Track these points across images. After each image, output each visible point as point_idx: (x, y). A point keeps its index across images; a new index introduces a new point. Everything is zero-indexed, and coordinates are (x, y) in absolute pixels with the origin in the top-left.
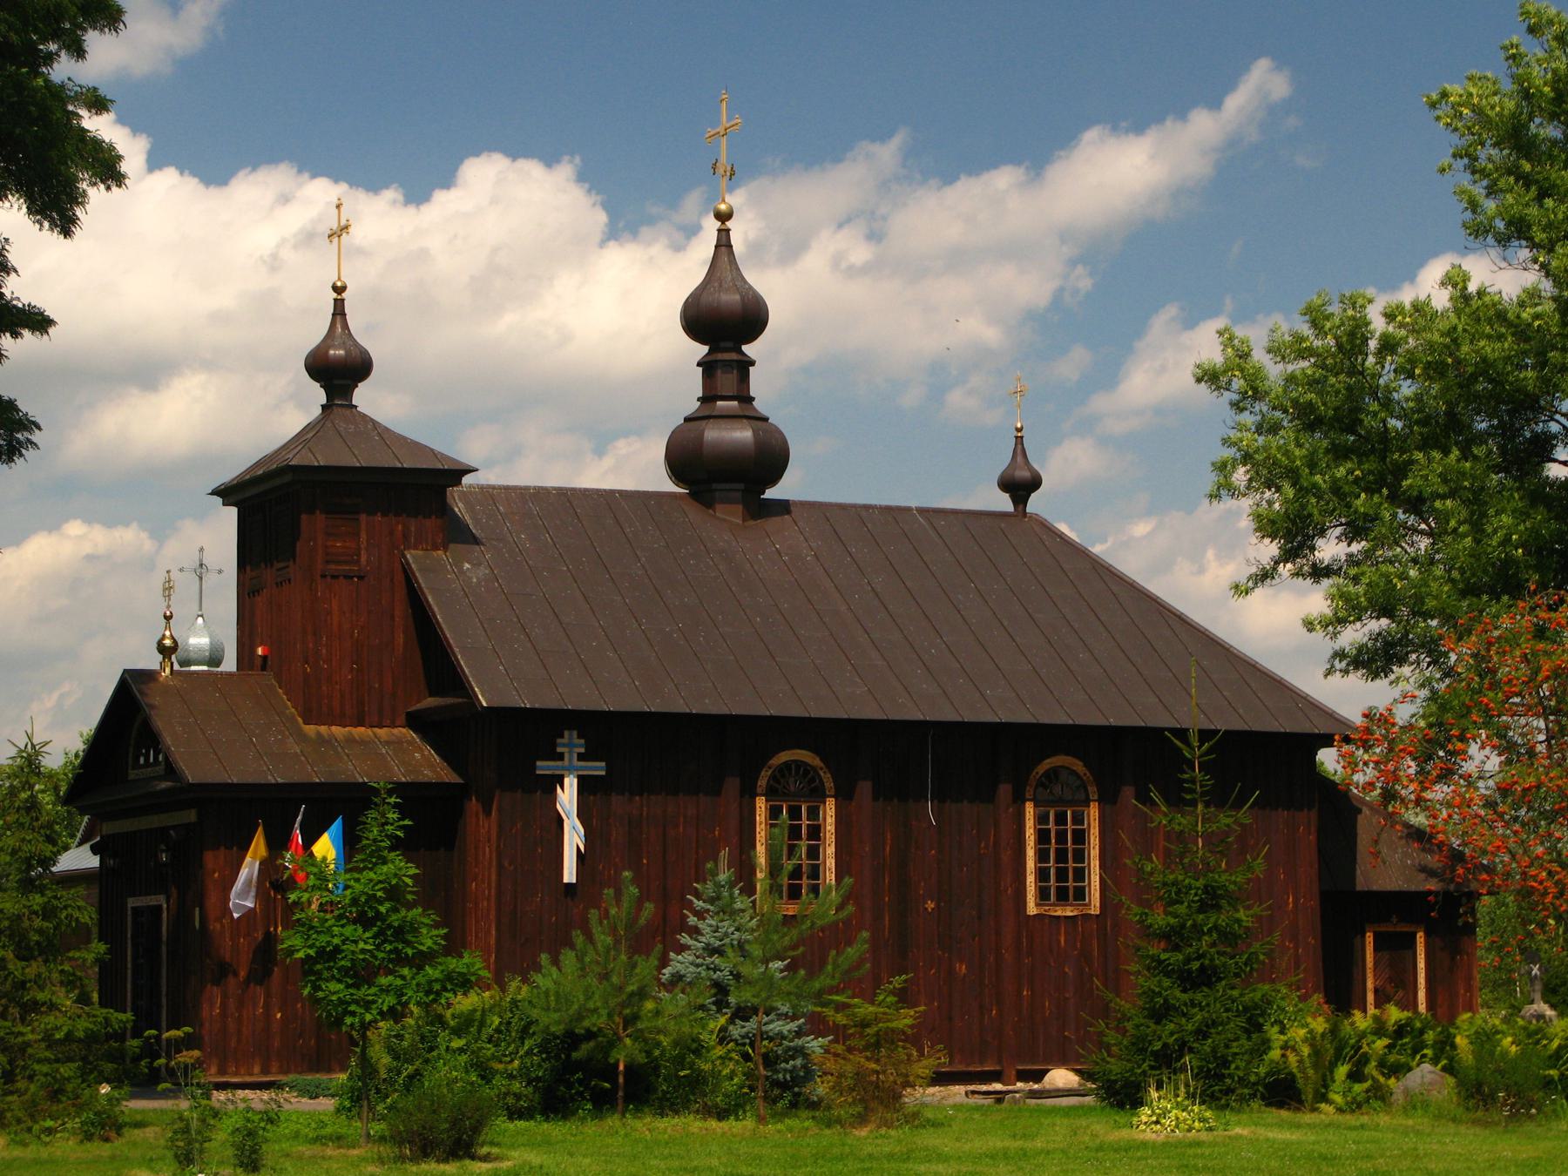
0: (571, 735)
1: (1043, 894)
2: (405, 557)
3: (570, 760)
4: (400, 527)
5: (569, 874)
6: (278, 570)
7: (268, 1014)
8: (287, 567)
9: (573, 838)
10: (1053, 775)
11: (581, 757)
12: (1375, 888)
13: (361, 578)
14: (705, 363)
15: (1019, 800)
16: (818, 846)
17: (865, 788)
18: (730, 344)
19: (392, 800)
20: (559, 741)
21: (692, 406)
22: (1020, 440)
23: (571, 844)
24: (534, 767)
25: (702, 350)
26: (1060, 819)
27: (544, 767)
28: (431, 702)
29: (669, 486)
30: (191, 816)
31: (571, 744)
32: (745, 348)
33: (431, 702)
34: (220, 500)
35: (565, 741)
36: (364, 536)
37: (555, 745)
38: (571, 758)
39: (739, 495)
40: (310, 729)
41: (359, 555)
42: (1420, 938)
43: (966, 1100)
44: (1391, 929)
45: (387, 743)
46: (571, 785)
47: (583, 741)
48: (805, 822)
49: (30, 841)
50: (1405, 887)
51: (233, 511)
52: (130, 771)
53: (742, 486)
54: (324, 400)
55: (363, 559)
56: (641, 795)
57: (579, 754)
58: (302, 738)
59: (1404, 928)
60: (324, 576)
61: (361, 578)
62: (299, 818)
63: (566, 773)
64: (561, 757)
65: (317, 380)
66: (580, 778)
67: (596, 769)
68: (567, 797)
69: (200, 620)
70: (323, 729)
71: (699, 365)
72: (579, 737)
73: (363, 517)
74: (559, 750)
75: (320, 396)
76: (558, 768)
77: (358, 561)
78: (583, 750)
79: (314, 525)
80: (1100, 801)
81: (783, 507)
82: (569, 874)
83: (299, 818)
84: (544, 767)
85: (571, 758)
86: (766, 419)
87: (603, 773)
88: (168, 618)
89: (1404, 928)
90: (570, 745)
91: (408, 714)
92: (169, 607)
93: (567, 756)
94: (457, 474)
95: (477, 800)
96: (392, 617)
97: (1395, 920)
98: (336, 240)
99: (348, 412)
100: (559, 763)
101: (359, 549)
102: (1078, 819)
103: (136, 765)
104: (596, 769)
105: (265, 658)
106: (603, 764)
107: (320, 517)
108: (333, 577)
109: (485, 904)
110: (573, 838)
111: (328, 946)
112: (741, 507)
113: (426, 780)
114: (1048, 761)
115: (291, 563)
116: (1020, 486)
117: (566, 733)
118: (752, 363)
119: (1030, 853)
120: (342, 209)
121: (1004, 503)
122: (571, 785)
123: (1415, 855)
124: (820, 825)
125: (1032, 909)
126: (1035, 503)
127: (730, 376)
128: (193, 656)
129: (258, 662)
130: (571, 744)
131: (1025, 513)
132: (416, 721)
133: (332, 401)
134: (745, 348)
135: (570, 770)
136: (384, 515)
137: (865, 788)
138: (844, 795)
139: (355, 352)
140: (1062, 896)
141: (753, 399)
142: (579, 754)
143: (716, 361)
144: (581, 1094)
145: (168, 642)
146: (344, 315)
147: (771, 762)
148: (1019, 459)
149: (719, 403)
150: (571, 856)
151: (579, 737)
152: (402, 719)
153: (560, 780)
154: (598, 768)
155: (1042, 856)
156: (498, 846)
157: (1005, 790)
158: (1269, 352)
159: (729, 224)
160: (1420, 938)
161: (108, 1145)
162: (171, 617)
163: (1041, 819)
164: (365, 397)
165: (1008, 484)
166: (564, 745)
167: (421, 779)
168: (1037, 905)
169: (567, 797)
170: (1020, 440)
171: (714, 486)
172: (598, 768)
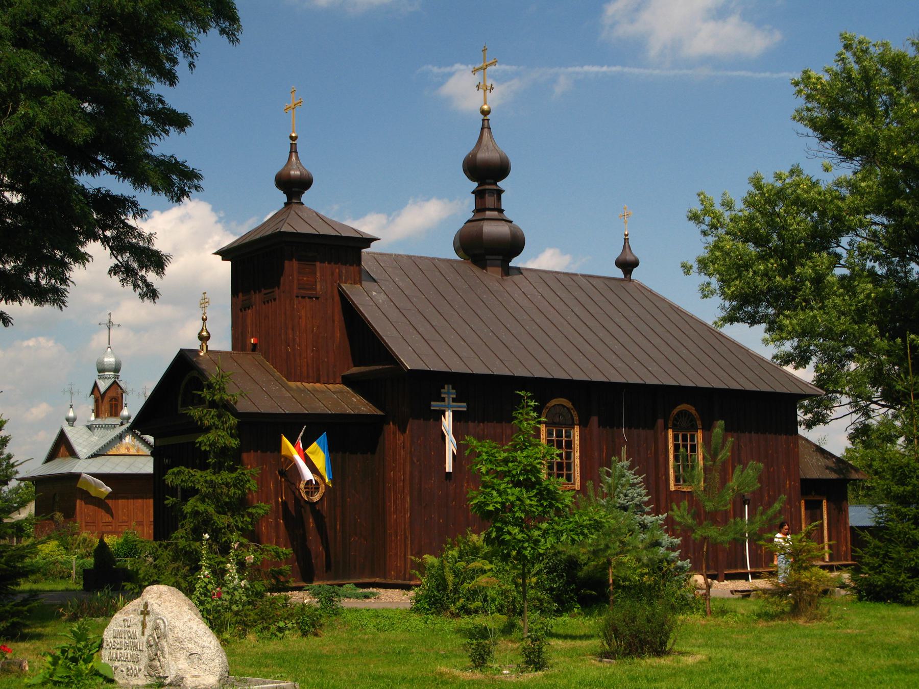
0: (448, 388)
1: (677, 480)
2: (341, 287)
3: (449, 403)
4: (337, 270)
5: (449, 467)
6: (265, 294)
8: (273, 292)
9: (451, 446)
10: (682, 413)
11: (454, 400)
12: (808, 477)
13: (317, 298)
14: (478, 191)
15: (666, 428)
16: (182, 489)
17: (594, 420)
18: (492, 181)
19: (533, 404)
20: (442, 390)
21: (470, 215)
22: (626, 240)
23: (449, 450)
24: (430, 405)
25: (475, 185)
26: (685, 439)
27: (435, 405)
28: (355, 370)
31: (448, 393)
33: (355, 370)
34: (220, 257)
35: (445, 390)
36: (318, 275)
37: (440, 393)
38: (449, 400)
39: (499, 262)
40: (292, 384)
41: (316, 286)
42: (824, 503)
43: (731, 596)
44: (812, 498)
45: (334, 393)
46: (449, 415)
47: (454, 391)
48: (564, 439)
49: (223, 437)
50: (821, 477)
53: (501, 257)
55: (318, 287)
56: (483, 423)
57: (453, 398)
58: (289, 389)
59: (818, 498)
60: (297, 297)
61: (317, 298)
62: (302, 433)
63: (446, 409)
64: (443, 400)
66: (454, 412)
67: (462, 407)
68: (447, 422)
69: (109, 349)
70: (299, 384)
71: (473, 193)
72: (453, 389)
73: (318, 264)
74: (443, 396)
75: (284, 198)
76: (442, 406)
77: (315, 289)
78: (454, 396)
79: (292, 267)
80: (702, 429)
81: (519, 270)
82: (449, 467)
83: (302, 433)
84: (435, 405)
85: (449, 400)
86: (511, 222)
87: (465, 409)
89: (818, 498)
90: (448, 393)
92: (204, 314)
93: (446, 399)
94: (367, 241)
95: (393, 424)
96: (333, 321)
97: (813, 494)
99: (301, 206)
100: (443, 403)
101: (316, 282)
102: (692, 439)
104: (462, 407)
105: (255, 345)
106: (465, 404)
107: (295, 264)
108: (303, 297)
109: (401, 484)
110: (451, 446)
111: (507, 502)
112: (500, 269)
113: (364, 413)
114: (685, 405)
115: (277, 288)
116: (627, 265)
117: (446, 386)
119: (671, 457)
121: (619, 273)
122: (449, 416)
123: (823, 462)
124: (571, 441)
126: (636, 274)
127: (492, 198)
128: (107, 367)
129: (249, 347)
130: (448, 393)
131: (630, 280)
132: (348, 381)
133: (292, 199)
135: (449, 407)
136: (329, 263)
137: (594, 420)
138: (584, 424)
139: (305, 173)
141: (503, 210)
142: (453, 398)
143: (485, 190)
144: (571, 598)
145: (204, 334)
146: (296, 152)
147: (548, 405)
148: (627, 250)
149: (487, 213)
150: (449, 457)
151: (453, 389)
152: (339, 380)
153: (443, 413)
154: (462, 407)
155: (676, 458)
156: (411, 451)
157: (660, 422)
158: (723, 205)
160: (824, 503)
161: (316, 638)
162: (206, 319)
163: (676, 438)
166: (445, 393)
167: (361, 412)
168: (675, 485)
169: (447, 422)
170: (626, 240)
171: (487, 257)
172: (462, 407)
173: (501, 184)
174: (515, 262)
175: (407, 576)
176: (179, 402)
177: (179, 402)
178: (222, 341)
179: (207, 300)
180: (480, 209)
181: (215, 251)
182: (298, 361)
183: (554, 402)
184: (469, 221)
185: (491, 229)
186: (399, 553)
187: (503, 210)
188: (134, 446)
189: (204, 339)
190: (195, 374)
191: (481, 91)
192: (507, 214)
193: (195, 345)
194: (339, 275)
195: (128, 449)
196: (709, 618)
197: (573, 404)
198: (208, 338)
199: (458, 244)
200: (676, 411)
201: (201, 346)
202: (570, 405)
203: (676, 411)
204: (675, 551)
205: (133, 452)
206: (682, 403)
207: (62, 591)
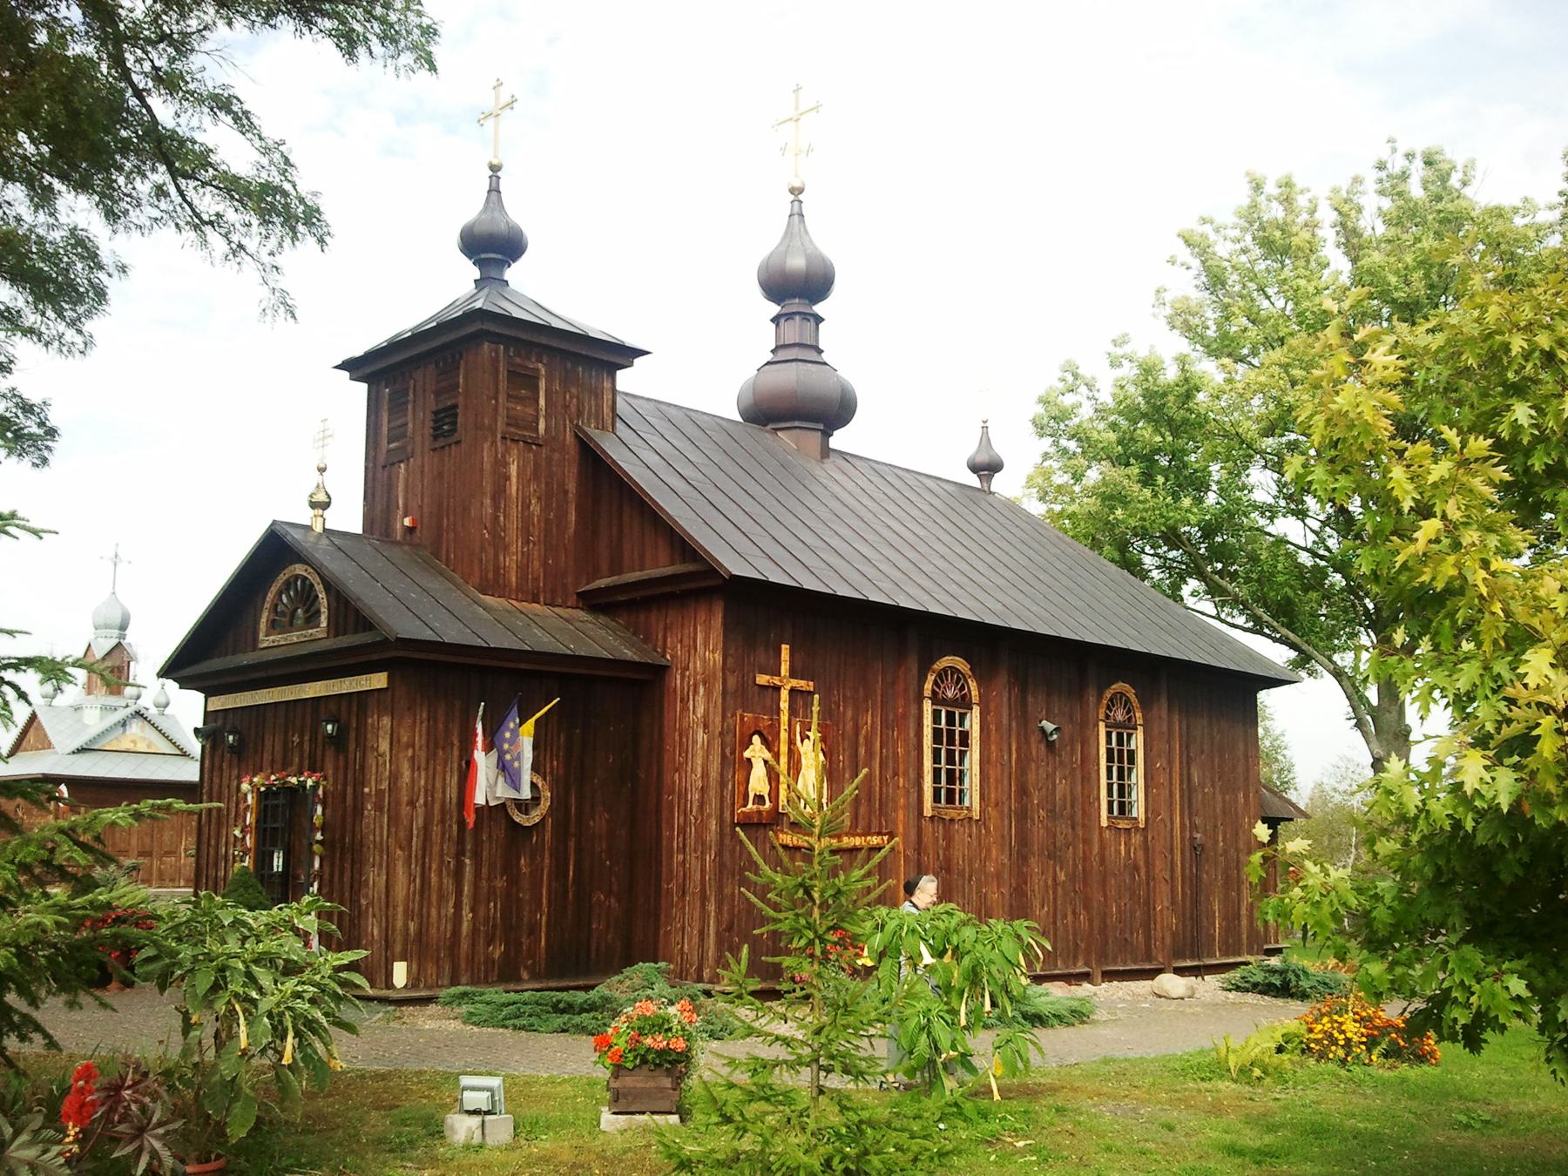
22: (985, 428)
25: (775, 309)
34: (347, 374)
40: (488, 599)
75: (476, 273)
88: (322, 470)
97: (525, 975)
121: (973, 480)
147: (935, 666)
152: (572, 600)
165: (975, 468)
170: (985, 428)
173: (818, 309)
174: (840, 440)
181: (339, 362)
183: (946, 661)
184: (768, 363)
188: (144, 739)
192: (825, 357)
193: (304, 515)
194: (578, 410)
195: (134, 742)
196: (847, 1078)
205: (142, 747)
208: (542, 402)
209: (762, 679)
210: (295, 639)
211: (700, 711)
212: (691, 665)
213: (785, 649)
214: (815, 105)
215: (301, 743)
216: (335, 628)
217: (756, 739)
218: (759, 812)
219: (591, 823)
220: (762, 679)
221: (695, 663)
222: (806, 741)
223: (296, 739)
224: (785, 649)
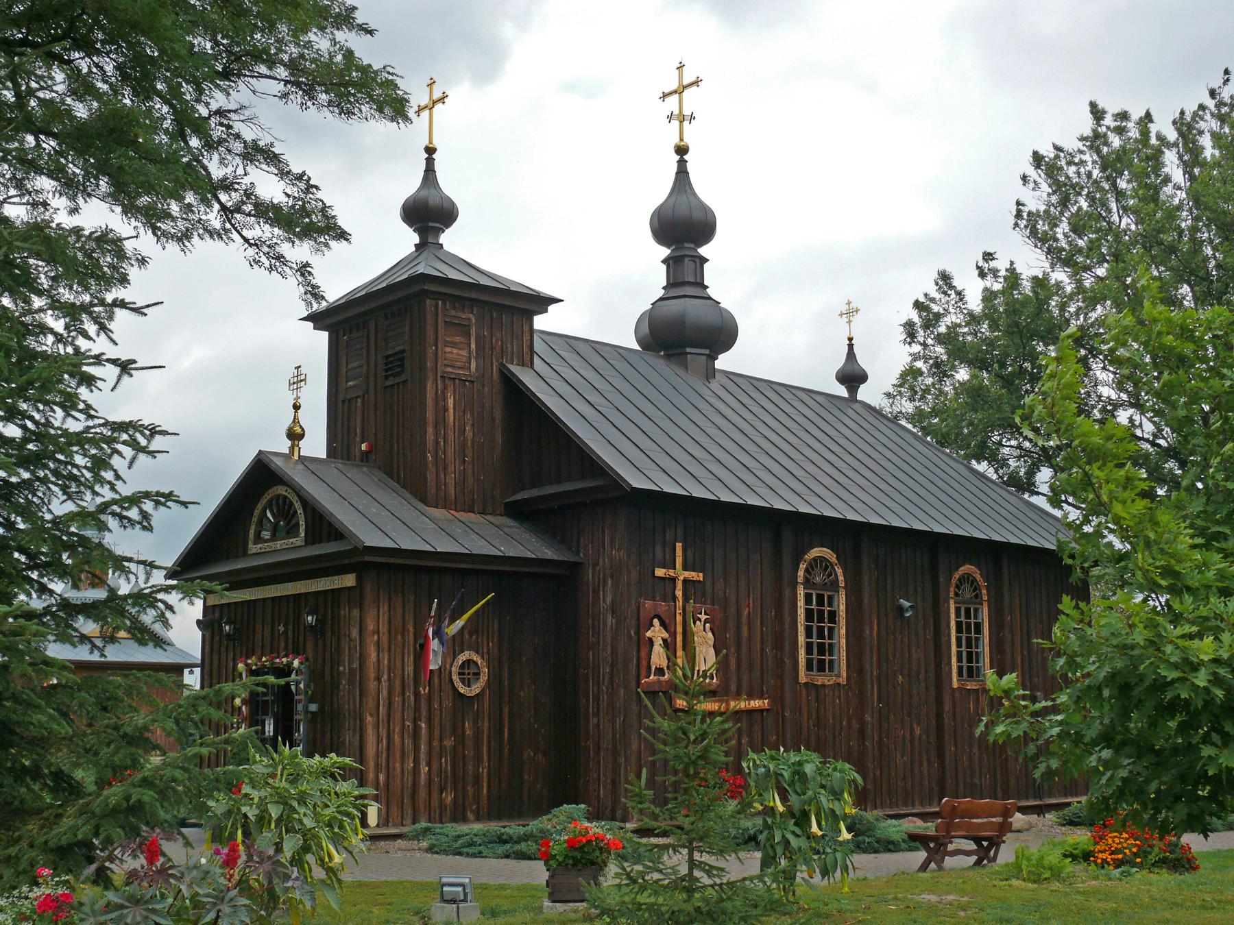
7: (416, 771)
21: (661, 293)
22: (851, 346)
25: (665, 252)
29: (637, 347)
30: (349, 580)
32: (699, 250)
34: (311, 325)
51: (325, 335)
52: (251, 545)
53: (707, 352)
54: (417, 240)
65: (410, 225)
75: (416, 238)
91: (507, 505)
98: (426, 113)
103: (258, 539)
118: (707, 260)
120: (435, 86)
121: (842, 391)
125: (803, 678)
134: (699, 250)
140: (821, 669)
141: (707, 287)
145: (298, 430)
159: (686, 157)
164: (451, 240)
170: (851, 346)
171: (688, 350)
173: (703, 251)
174: (724, 362)
175: (619, 813)
176: (251, 536)
177: (251, 536)
178: (316, 445)
179: (303, 377)
180: (673, 283)
182: (443, 477)
183: (815, 552)
184: (661, 299)
185: (689, 308)
186: (602, 778)
187: (707, 287)
189: (295, 435)
190: (281, 490)
191: (676, 123)
192: (711, 292)
193: (284, 446)
197: (837, 558)
198: (301, 436)
199: (645, 329)
200: (957, 576)
201: (292, 448)
202: (834, 559)
203: (957, 576)
204: (1042, 775)
206: (964, 563)
207: (714, 634)
208: (473, 346)
209: (660, 572)
210: (279, 547)
211: (609, 599)
212: (601, 562)
213: (679, 545)
214: (694, 79)
215: (285, 632)
216: (311, 540)
217: (656, 622)
218: (659, 681)
219: (522, 694)
220: (660, 572)
221: (604, 561)
222: (698, 622)
223: (282, 629)
224: (679, 545)
